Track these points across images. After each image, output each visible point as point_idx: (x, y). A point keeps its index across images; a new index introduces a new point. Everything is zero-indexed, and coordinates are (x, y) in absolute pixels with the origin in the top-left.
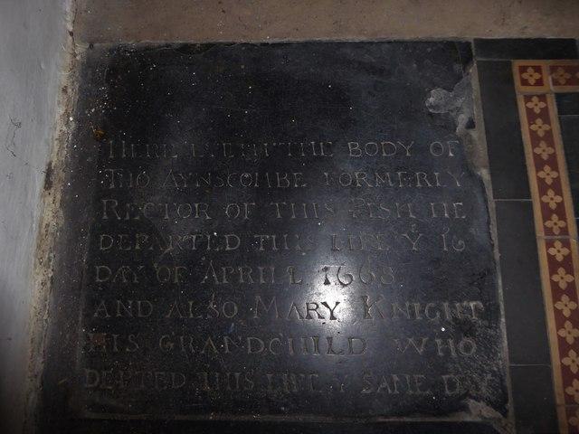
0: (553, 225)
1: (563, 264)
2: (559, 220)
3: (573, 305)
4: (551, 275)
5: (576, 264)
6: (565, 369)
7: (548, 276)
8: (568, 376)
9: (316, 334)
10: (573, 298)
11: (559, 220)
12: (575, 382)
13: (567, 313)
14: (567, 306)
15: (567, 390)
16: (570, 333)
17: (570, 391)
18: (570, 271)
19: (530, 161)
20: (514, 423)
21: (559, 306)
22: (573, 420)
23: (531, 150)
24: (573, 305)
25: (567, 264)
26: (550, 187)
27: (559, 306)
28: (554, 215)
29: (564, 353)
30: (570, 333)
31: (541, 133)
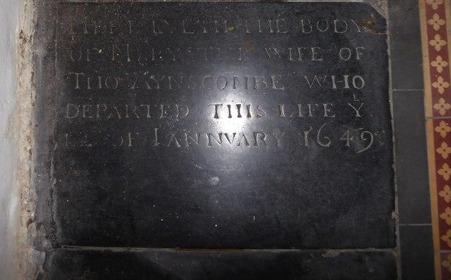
0: (435, 44)
1: (440, 53)
2: (444, 81)
3: (446, 85)
4: (438, 192)
5: (447, 12)
6: (441, 200)
7: (436, 191)
8: (443, 205)
9: (250, 89)
10: (446, 79)
11: (444, 81)
12: (448, 209)
13: (441, 91)
14: (441, 85)
15: (432, 64)
16: (445, 150)
17: (445, 238)
18: (445, 58)
19: (425, 52)
20: (386, 3)
21: (434, 64)
22: (446, 264)
23: (425, 22)
24: (446, 85)
25: (443, 32)
26: (440, 75)
27: (434, 64)
28: (436, 30)
29: (440, 188)
30: (442, 106)
31: (440, 70)
